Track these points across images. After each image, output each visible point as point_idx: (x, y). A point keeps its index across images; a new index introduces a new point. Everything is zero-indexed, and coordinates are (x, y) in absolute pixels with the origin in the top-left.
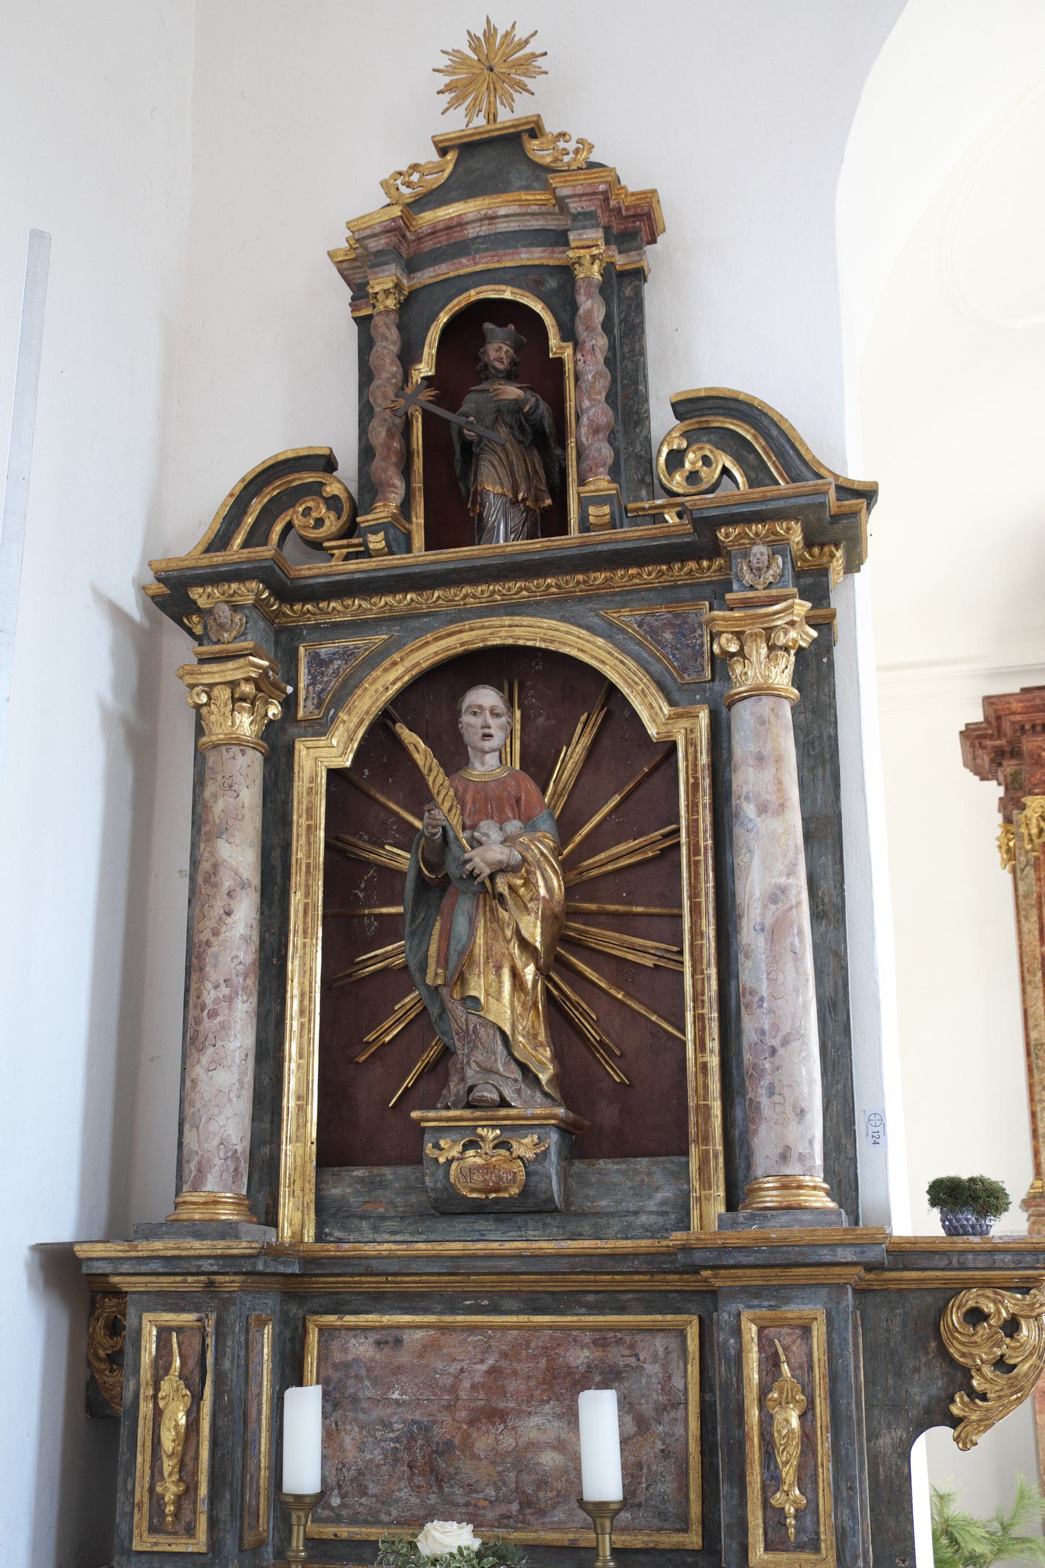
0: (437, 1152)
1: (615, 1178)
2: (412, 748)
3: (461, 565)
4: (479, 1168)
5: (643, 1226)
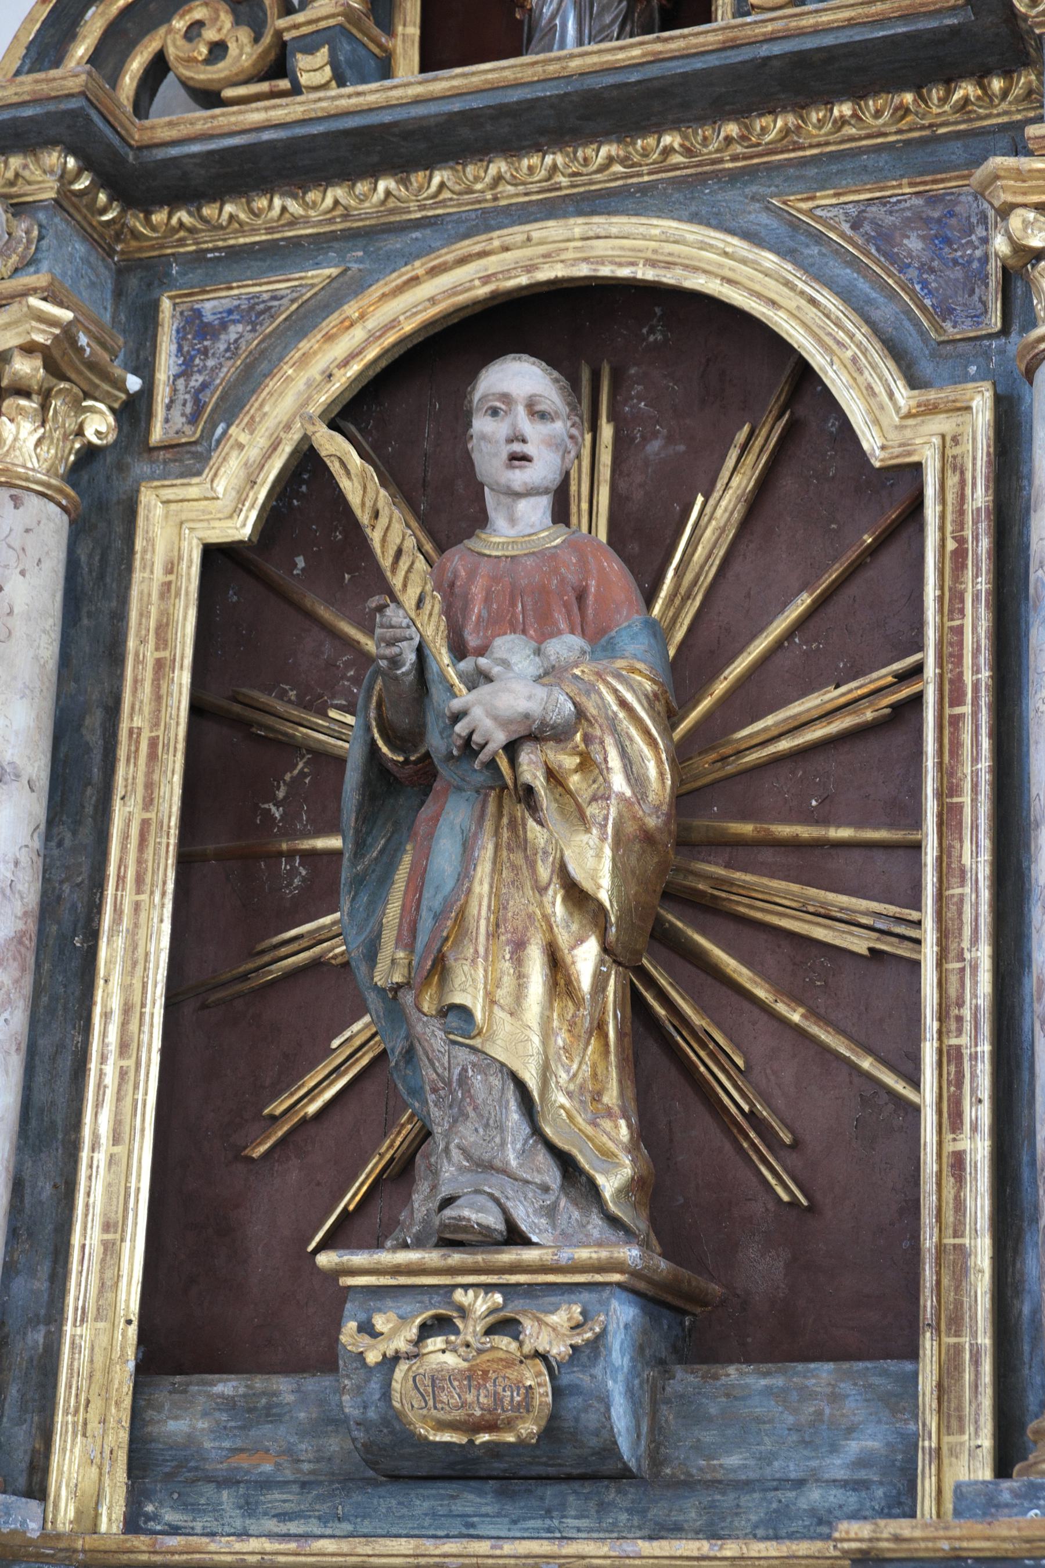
0: (366, 1339)
1: (760, 1407)
2: (335, 467)
3: (476, 103)
4: (451, 1376)
5: (812, 1512)
